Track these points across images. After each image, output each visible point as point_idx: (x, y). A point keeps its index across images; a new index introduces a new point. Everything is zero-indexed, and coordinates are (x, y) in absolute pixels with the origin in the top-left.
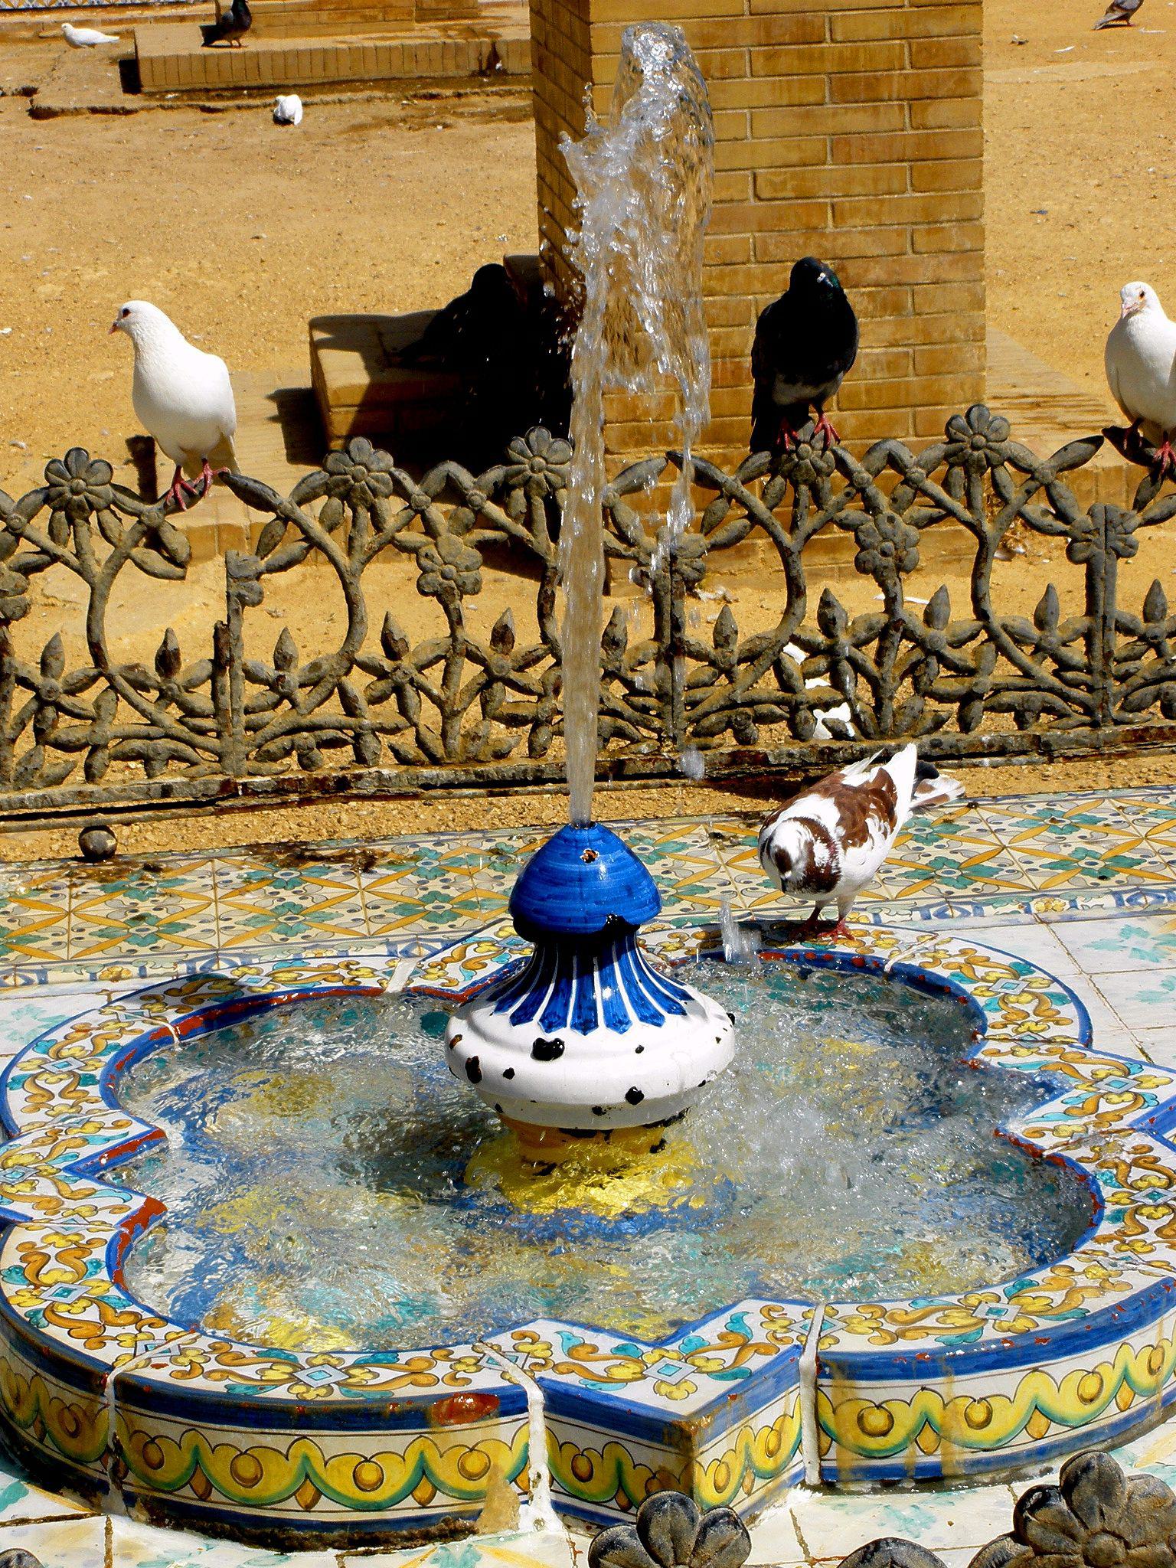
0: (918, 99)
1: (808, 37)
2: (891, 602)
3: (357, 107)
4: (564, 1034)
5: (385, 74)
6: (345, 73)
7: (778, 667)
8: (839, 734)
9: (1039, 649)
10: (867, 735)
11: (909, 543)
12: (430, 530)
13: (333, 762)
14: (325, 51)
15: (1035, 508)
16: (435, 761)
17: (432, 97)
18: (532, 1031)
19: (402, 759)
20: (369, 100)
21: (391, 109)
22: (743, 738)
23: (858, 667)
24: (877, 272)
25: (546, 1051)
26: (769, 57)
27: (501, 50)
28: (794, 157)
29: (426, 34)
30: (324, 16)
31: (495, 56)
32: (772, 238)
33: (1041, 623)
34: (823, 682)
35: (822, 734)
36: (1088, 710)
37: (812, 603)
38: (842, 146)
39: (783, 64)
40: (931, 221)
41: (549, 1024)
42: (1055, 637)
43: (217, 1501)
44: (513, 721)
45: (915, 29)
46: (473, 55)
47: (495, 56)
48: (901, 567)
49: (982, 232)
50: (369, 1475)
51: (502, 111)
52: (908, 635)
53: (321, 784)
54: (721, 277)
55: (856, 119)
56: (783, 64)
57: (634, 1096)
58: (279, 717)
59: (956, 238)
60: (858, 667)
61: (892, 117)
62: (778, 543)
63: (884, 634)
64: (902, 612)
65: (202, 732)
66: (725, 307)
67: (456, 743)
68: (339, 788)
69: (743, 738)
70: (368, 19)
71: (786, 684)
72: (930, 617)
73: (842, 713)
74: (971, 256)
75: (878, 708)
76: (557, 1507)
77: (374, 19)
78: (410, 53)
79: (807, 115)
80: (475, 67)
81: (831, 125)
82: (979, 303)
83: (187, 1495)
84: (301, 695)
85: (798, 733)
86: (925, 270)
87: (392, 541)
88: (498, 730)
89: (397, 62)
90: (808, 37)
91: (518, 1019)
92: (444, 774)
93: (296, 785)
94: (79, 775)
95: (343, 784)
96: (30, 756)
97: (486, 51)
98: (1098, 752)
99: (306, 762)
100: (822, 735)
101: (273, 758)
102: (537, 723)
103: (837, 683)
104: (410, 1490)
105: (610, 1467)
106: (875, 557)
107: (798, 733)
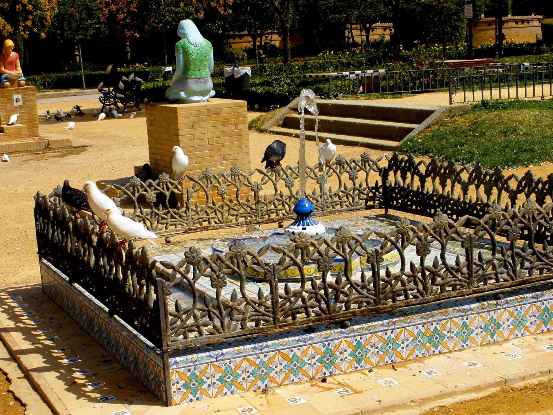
0: (237, 124)
1: (216, 113)
2: (291, 192)
3: (20, 158)
4: (306, 226)
5: (23, 150)
6: (14, 150)
7: (274, 204)
8: (284, 215)
9: (313, 199)
10: (288, 214)
11: (293, 182)
12: (219, 183)
13: (205, 224)
14: (9, 145)
15: (312, 175)
16: (221, 223)
17: (38, 154)
18: (301, 227)
19: (216, 223)
20: (23, 155)
21: (30, 157)
22: (269, 216)
23: (287, 203)
24: (231, 157)
25: (304, 229)
26: (210, 117)
27: (50, 143)
28: (215, 136)
29: (30, 140)
30: (6, 137)
31: (49, 144)
32: (212, 152)
33: (313, 194)
34: (281, 206)
35: (281, 215)
36: (321, 208)
37: (279, 192)
38: (224, 134)
39: (212, 119)
40: (240, 147)
41: (303, 225)
42: (316, 196)
43: (289, 277)
44: (233, 215)
45: (235, 111)
46: (44, 144)
47: (49, 144)
48: (292, 186)
49: (249, 149)
50: (309, 271)
51: (57, 155)
52: (294, 197)
53: (204, 228)
54: (203, 160)
55: (226, 129)
56: (212, 119)
57: (317, 234)
58: (196, 217)
59: (245, 150)
60: (287, 203)
61: (232, 128)
62: (273, 182)
63: (290, 197)
64: (293, 194)
65: (184, 220)
66: (204, 165)
67: (224, 219)
68: (206, 228)
69: (269, 216)
70: (16, 137)
71: (275, 207)
72: (297, 194)
73: (284, 211)
74: (247, 154)
75: (290, 210)
76: (331, 275)
77: (17, 137)
78: (29, 145)
79: (217, 128)
80: (44, 147)
81: (221, 130)
82: (250, 162)
83: (284, 277)
84: (200, 213)
85: (277, 215)
86: (239, 156)
87: (214, 186)
88: (231, 218)
89: (26, 146)
90: (216, 113)
91: (298, 225)
92: (223, 224)
93: (200, 228)
94: (165, 228)
95: (207, 227)
96: (157, 226)
97: (47, 143)
98: (324, 215)
99: (201, 224)
100: (281, 215)
101: (195, 224)
102: (237, 216)
103: (283, 206)
104: (314, 273)
105: (339, 267)
106: (288, 184)
107: (277, 215)
